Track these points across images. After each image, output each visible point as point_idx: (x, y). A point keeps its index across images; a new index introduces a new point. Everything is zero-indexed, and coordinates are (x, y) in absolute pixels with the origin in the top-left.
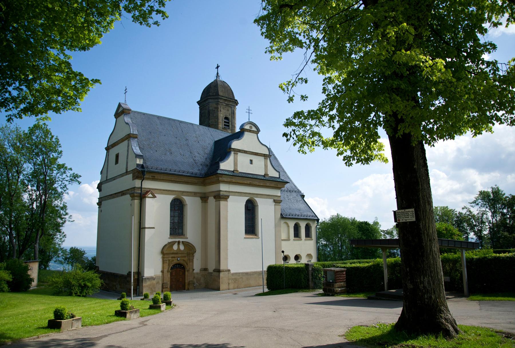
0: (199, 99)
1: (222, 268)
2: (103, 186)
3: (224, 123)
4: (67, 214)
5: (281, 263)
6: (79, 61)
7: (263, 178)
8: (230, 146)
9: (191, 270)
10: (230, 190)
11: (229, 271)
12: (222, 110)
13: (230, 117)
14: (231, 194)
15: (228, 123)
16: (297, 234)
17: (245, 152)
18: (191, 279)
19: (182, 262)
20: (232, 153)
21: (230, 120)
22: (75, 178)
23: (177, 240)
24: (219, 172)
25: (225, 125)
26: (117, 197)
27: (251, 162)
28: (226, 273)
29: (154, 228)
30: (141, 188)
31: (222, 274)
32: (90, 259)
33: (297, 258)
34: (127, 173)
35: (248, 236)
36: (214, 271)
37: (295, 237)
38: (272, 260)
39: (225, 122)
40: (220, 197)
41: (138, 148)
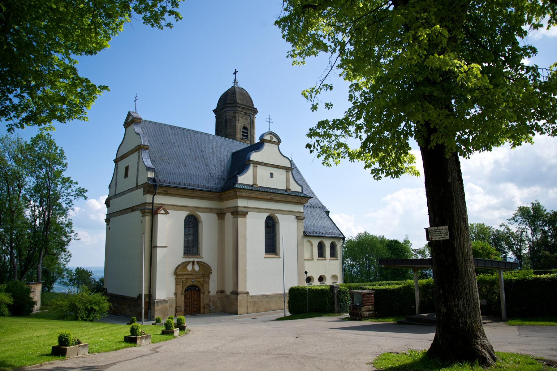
0: (215, 107)
1: (240, 290)
2: (111, 201)
3: (242, 134)
4: (72, 232)
5: (304, 284)
6: (85, 66)
7: (284, 193)
8: (249, 158)
9: (207, 293)
10: (249, 206)
11: (248, 293)
12: (240, 119)
13: (249, 127)
14: (249, 210)
15: (247, 133)
16: (321, 254)
17: (265, 165)
18: (207, 302)
19: (197, 284)
20: (251, 165)
21: (249, 130)
22: (81, 192)
23: (192, 260)
24: (237, 186)
25: (243, 135)
26: (127, 213)
27: (272, 175)
28: (245, 295)
29: (166, 247)
30: (153, 203)
31: (240, 297)
32: (97, 280)
33: (321, 279)
34: (137, 187)
35: (268, 256)
36: (232, 293)
37: (319, 256)
38: (294, 282)
39: (243, 132)
40: (238, 213)
41: (149, 160)
